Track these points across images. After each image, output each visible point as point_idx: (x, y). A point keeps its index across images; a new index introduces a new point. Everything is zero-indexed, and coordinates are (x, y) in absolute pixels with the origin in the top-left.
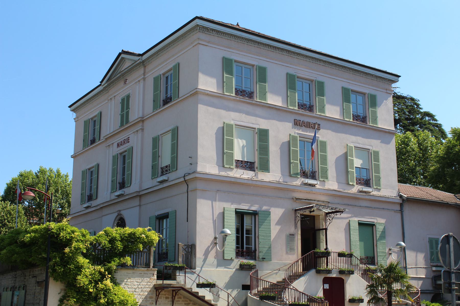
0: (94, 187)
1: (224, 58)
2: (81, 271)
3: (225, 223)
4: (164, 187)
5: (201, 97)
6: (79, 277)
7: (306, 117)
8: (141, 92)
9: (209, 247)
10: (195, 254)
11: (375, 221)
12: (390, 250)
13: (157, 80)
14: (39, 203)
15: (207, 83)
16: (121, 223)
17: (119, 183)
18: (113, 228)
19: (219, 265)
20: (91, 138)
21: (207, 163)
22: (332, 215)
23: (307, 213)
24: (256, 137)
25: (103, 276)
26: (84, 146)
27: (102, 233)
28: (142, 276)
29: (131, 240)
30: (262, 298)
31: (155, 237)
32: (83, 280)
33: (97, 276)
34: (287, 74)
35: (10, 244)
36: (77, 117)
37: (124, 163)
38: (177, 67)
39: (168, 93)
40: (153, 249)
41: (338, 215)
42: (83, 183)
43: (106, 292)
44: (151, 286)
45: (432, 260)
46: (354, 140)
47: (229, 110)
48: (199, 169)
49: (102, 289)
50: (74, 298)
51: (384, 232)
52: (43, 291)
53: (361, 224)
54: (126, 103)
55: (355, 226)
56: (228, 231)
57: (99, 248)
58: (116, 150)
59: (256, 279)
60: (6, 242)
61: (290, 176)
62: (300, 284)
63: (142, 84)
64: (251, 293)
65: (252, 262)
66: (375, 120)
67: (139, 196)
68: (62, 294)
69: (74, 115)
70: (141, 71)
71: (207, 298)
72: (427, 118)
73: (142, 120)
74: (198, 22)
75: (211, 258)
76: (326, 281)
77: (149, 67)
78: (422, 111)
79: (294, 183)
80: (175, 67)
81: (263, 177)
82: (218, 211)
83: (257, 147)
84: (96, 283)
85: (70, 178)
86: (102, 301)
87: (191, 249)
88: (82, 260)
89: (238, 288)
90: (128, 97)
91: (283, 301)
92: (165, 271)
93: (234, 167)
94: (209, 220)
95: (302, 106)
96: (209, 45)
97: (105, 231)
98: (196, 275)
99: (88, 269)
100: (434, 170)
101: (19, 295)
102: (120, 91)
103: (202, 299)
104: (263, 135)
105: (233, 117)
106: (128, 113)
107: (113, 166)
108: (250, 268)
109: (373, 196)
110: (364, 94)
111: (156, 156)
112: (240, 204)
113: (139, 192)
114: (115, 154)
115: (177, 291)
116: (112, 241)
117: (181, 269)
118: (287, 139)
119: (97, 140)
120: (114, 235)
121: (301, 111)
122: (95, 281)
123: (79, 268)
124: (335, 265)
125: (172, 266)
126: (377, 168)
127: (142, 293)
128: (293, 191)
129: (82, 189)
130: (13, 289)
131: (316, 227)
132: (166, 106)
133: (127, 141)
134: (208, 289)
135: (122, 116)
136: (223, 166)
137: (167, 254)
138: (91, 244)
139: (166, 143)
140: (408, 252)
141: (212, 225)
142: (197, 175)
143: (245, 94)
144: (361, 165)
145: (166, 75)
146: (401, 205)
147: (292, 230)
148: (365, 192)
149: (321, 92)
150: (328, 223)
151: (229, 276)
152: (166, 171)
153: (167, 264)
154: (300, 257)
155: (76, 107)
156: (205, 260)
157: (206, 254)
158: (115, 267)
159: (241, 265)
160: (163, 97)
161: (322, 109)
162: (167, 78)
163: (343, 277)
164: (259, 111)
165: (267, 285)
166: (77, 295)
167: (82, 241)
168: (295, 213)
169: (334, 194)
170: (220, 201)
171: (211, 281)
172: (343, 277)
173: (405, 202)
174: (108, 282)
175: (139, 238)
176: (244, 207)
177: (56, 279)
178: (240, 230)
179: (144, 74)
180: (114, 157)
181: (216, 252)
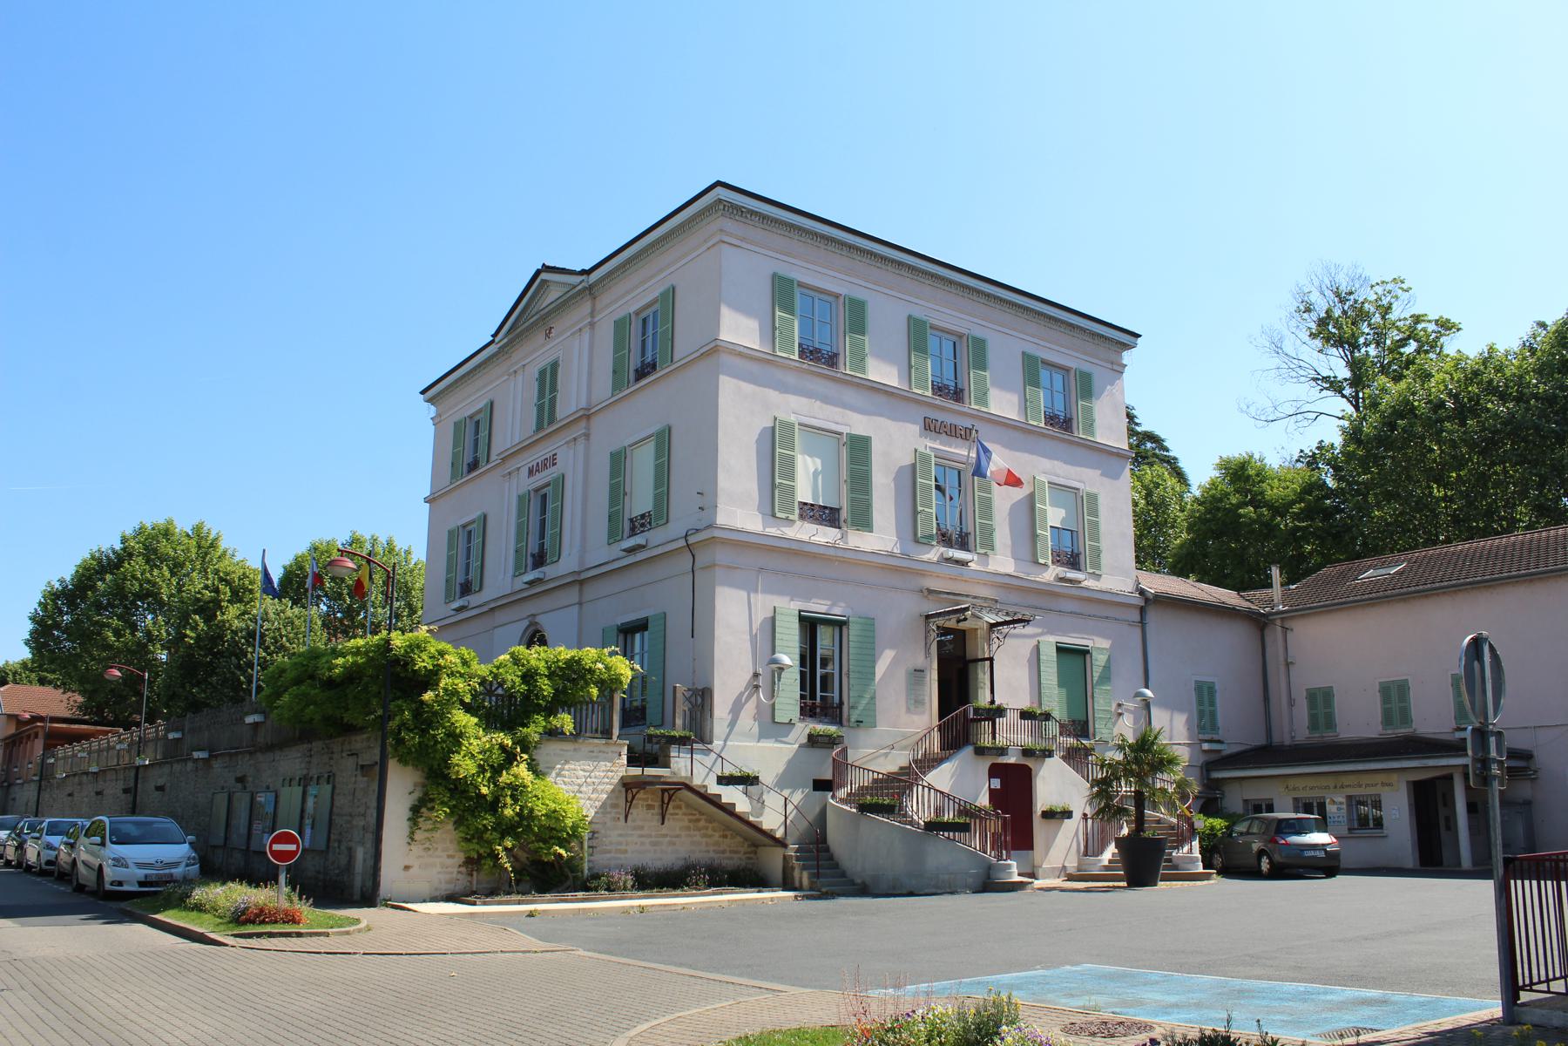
0: (475, 564)
1: (774, 276)
2: (460, 745)
3: (778, 643)
4: (637, 561)
5: (725, 358)
6: (456, 758)
7: (950, 413)
8: (584, 354)
9: (742, 694)
10: (711, 710)
11: (1090, 643)
12: (1119, 705)
13: (621, 326)
14: (350, 606)
15: (739, 329)
16: (535, 637)
17: (533, 555)
18: (528, 647)
19: (763, 735)
20: (468, 459)
21: (739, 509)
22: (1005, 629)
23: (951, 623)
24: (844, 452)
25: (510, 758)
26: (454, 476)
27: (505, 657)
28: (593, 757)
29: (571, 676)
30: (863, 808)
31: (624, 669)
32: (464, 765)
33: (497, 757)
34: (910, 317)
35: (298, 681)
36: (439, 415)
37: (543, 511)
38: (670, 296)
39: (647, 355)
40: (618, 697)
41: (1019, 629)
42: (449, 558)
43: (517, 791)
44: (616, 781)
45: (1201, 728)
46: (1041, 468)
47: (786, 392)
48: (721, 520)
49: (510, 786)
50: (443, 803)
51: (1107, 668)
52: (375, 786)
53: (1062, 650)
54: (548, 379)
55: (1049, 654)
56: (786, 660)
57: (500, 691)
58: (526, 483)
59: (841, 766)
60: (290, 675)
61: (917, 541)
62: (942, 777)
63: (586, 336)
64: (833, 797)
65: (832, 729)
66: (1090, 427)
67: (579, 582)
68: (418, 794)
69: (432, 410)
70: (586, 307)
71: (738, 809)
72: (1149, 445)
73: (587, 415)
74: (720, 192)
75: (747, 720)
76: (994, 771)
77: (605, 299)
78: (1139, 429)
79: (925, 557)
80: (664, 295)
81: (859, 541)
82: (761, 615)
83: (845, 475)
84: (497, 771)
85: (419, 554)
86: (508, 812)
87: (702, 699)
88: (462, 719)
89: (804, 787)
90: (554, 366)
91: (905, 815)
92: (648, 747)
93: (795, 516)
94: (742, 634)
95: (939, 389)
96: (743, 245)
97: (512, 655)
98: (713, 756)
99: (476, 742)
100: (1182, 546)
101: (318, 795)
102: (536, 354)
103: (729, 810)
104: (859, 448)
105: (795, 408)
106: (553, 402)
107: (520, 515)
108: (830, 742)
109: (1087, 589)
110: (1067, 370)
111: (617, 493)
112: (808, 599)
113: (579, 573)
114: (522, 490)
115: (672, 793)
116: (529, 676)
117: (683, 741)
118: (908, 460)
119: (482, 462)
120: (533, 662)
121: (939, 401)
122: (492, 767)
123: (455, 738)
124: (1012, 735)
125: (663, 736)
126: (1095, 526)
127: (594, 796)
128: (922, 574)
129: (449, 571)
130: (305, 781)
131: (969, 656)
132: (643, 382)
133: (553, 461)
134: (741, 787)
135: (540, 408)
136: (774, 515)
137: (643, 709)
138: (483, 682)
139: (643, 465)
140: (1154, 711)
141: (748, 645)
142: (717, 533)
143: (819, 356)
144: (1063, 521)
145: (643, 315)
146: (1142, 610)
147: (920, 661)
148: (1070, 581)
149: (981, 364)
150: (995, 647)
151: (786, 759)
152: (643, 525)
153: (652, 731)
154: (936, 722)
155: (435, 393)
156: (732, 724)
157: (736, 709)
158: (536, 737)
159: (810, 736)
160: (635, 362)
161: (983, 399)
162: (644, 320)
163: (1030, 763)
164: (849, 395)
165: (866, 780)
166: (452, 798)
167: (462, 675)
168: (927, 624)
169: (1007, 584)
170: (764, 591)
171: (749, 769)
172: (1030, 763)
173: (1151, 603)
174: (522, 770)
175: (591, 671)
176: (818, 607)
177: (403, 761)
178: (808, 658)
179: (592, 314)
180: (520, 498)
181: (758, 707)
